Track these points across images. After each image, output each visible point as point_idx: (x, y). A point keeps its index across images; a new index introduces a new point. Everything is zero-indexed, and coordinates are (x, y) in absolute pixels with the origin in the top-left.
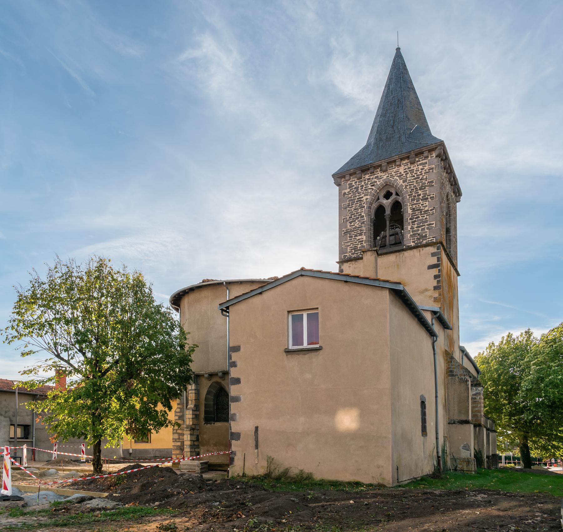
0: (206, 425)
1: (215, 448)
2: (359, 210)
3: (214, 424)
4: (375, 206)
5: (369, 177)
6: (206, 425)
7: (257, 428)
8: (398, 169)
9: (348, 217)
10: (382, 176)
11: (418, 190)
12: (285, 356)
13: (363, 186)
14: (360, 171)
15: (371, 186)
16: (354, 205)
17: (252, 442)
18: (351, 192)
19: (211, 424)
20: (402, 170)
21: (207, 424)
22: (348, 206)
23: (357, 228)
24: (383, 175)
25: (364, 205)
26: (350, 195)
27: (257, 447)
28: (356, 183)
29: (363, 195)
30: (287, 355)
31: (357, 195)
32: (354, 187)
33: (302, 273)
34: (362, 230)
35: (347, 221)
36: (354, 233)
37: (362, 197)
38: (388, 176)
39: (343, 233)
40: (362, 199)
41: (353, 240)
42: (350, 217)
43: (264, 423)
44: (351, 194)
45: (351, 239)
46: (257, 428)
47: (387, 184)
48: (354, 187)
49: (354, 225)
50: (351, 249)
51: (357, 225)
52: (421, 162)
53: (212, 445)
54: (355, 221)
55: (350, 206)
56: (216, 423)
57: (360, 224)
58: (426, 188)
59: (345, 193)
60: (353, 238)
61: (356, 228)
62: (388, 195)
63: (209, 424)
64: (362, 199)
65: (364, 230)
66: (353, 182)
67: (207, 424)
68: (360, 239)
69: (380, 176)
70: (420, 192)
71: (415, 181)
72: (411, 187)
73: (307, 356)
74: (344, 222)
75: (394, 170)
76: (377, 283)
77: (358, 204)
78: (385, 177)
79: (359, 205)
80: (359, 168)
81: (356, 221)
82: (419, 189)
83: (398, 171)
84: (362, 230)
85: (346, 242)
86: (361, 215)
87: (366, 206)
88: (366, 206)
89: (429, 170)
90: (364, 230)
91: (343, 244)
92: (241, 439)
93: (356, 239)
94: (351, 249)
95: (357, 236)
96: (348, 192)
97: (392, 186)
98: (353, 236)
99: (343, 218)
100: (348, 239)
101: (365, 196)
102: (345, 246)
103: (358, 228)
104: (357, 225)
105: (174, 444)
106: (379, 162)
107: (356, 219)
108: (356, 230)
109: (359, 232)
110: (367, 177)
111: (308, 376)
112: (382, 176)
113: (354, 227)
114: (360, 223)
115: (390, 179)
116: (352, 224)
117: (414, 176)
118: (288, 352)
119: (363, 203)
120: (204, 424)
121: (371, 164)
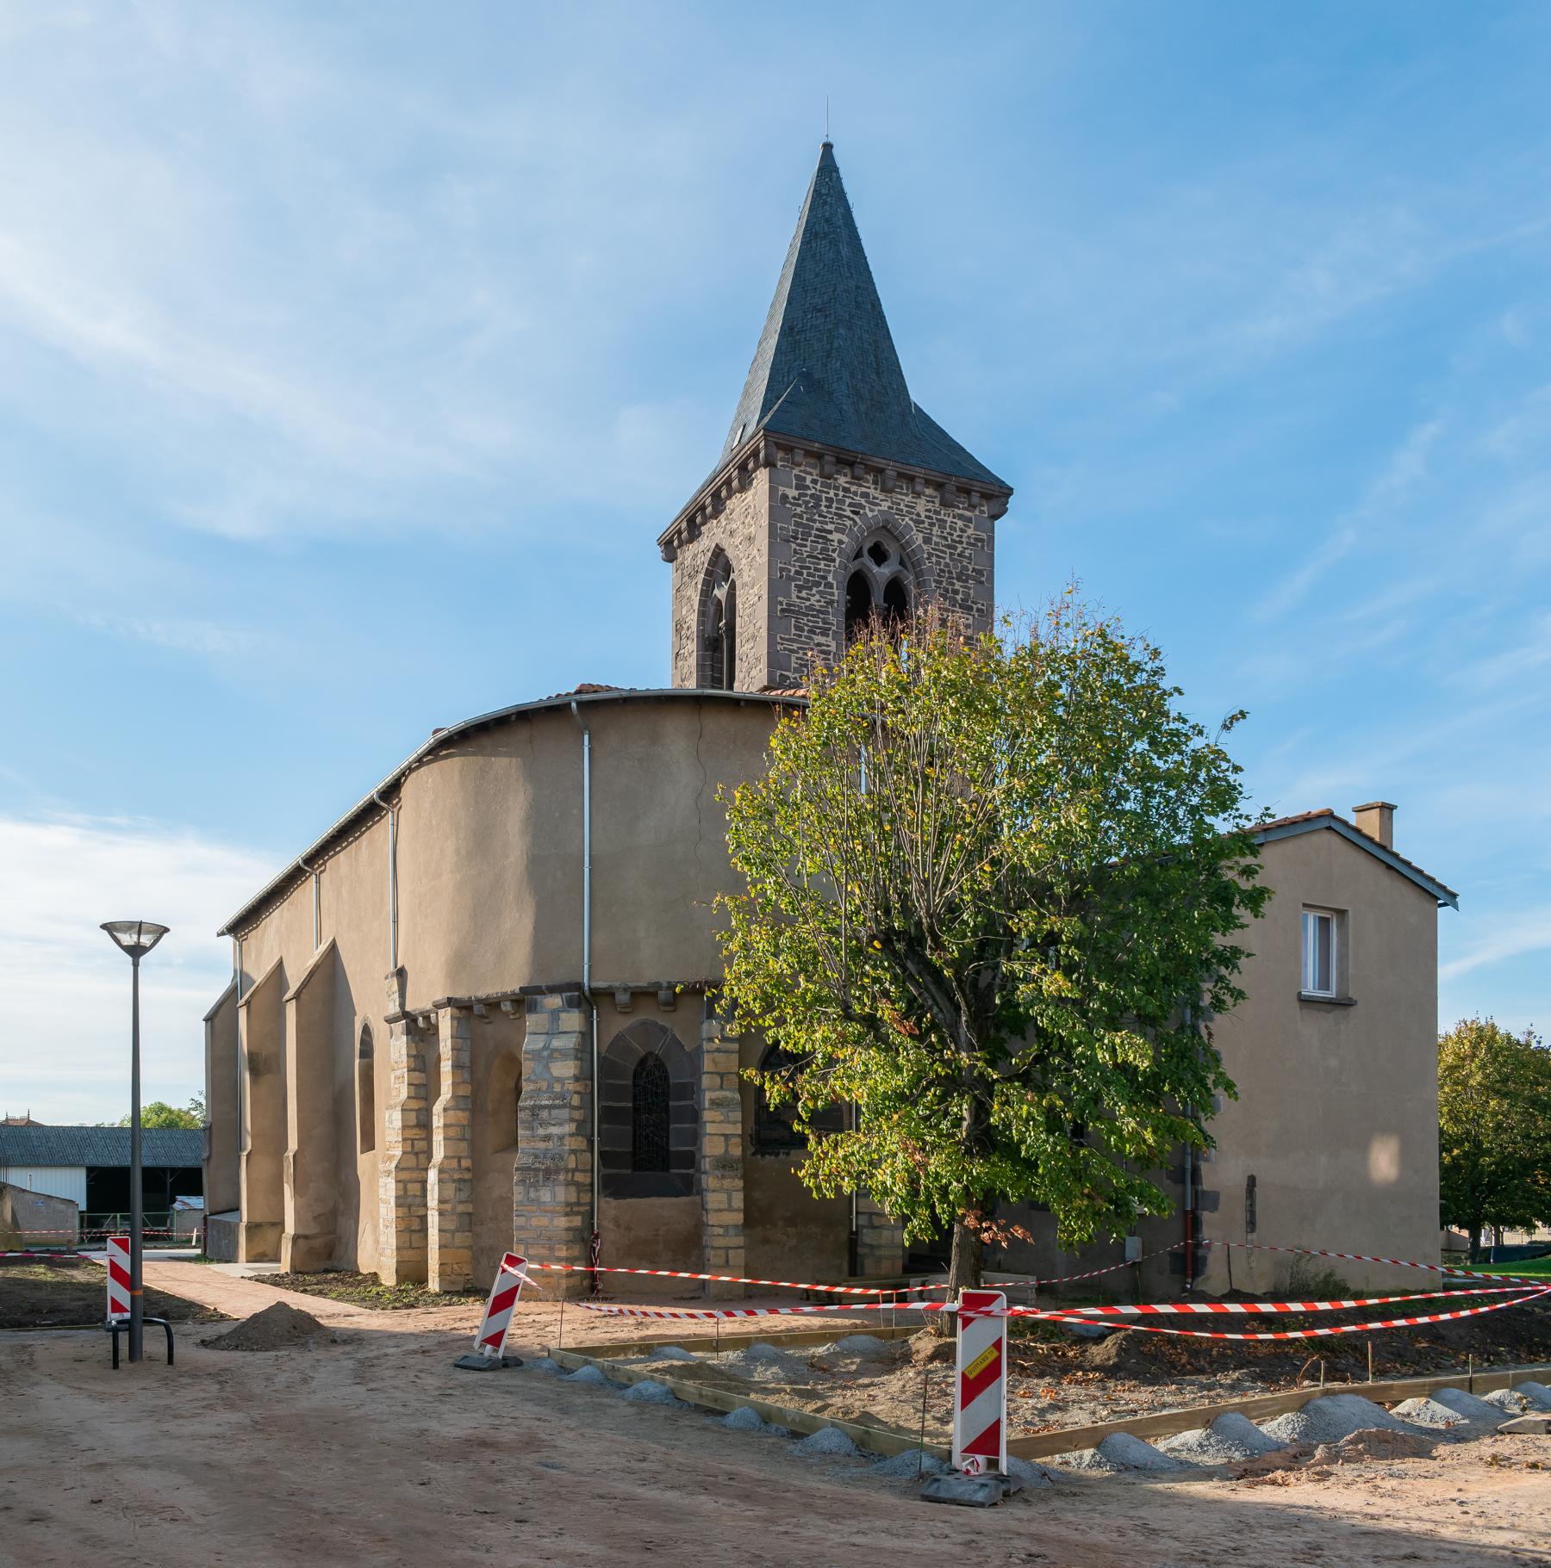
0: (759, 1157)
1: (791, 1230)
2: (822, 562)
3: (788, 1154)
4: (853, 567)
5: (848, 486)
6: (759, 1157)
7: (1252, 1181)
8: (914, 500)
9: (793, 570)
10: (877, 499)
11: (953, 578)
12: (1298, 1009)
13: (830, 500)
14: (833, 459)
15: (853, 512)
16: (809, 543)
17: (1241, 1216)
18: (801, 502)
19: (777, 1155)
20: (921, 506)
21: (763, 1156)
22: (792, 537)
23: (814, 610)
24: (881, 497)
25: (835, 555)
26: (799, 510)
27: (1251, 1225)
28: (814, 482)
29: (830, 527)
30: (1301, 1009)
31: (816, 517)
32: (809, 492)
33: (1327, 821)
34: (828, 624)
35: (790, 579)
36: (808, 620)
37: (830, 532)
38: (892, 508)
39: (779, 607)
40: (829, 536)
41: (803, 639)
42: (797, 572)
43: (1270, 1172)
44: (800, 506)
45: (800, 636)
46: (1252, 1181)
47: (886, 528)
48: (809, 492)
49: (809, 600)
50: (801, 664)
51: (816, 604)
52: (960, 512)
53: (780, 1223)
54: (810, 589)
55: (799, 541)
56: (793, 1152)
57: (822, 604)
58: (970, 581)
59: (785, 497)
60: (806, 633)
61: (811, 608)
62: (879, 555)
63: (770, 1154)
64: (829, 536)
65: (833, 624)
66: (809, 478)
67: (763, 1156)
68: (823, 645)
69: (874, 498)
70: (958, 585)
71: (948, 551)
72: (938, 563)
73: (1331, 1016)
74: (781, 577)
75: (907, 499)
76: (1429, 887)
77: (820, 546)
78: (885, 506)
79: (822, 549)
80: (835, 450)
81: (814, 591)
82: (955, 576)
83: (913, 507)
84: (828, 624)
85: (787, 637)
86: (825, 578)
87: (838, 560)
88: (838, 560)
89: (975, 539)
90: (833, 624)
91: (779, 640)
92: (1220, 1207)
93: (812, 639)
94: (799, 662)
95: (815, 633)
96: (794, 498)
97: (897, 539)
98: (806, 628)
99: (779, 565)
100: (793, 631)
101: (837, 530)
102: (785, 649)
103: (818, 611)
104: (816, 604)
105: (568, 1225)
106: (883, 461)
107: (813, 586)
108: (812, 616)
109: (821, 625)
110: (842, 480)
111: (1333, 1062)
112: (877, 499)
113: (808, 603)
114: (823, 600)
115: (897, 517)
116: (804, 594)
117: (946, 539)
118: (1306, 1002)
119: (831, 548)
120: (753, 1154)
121: (865, 457)
